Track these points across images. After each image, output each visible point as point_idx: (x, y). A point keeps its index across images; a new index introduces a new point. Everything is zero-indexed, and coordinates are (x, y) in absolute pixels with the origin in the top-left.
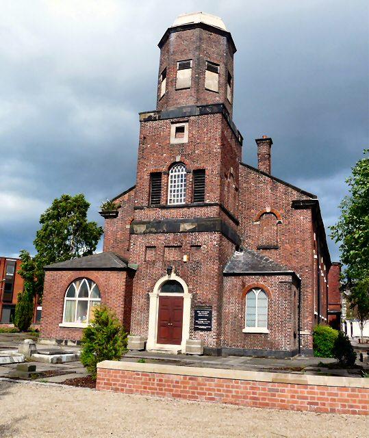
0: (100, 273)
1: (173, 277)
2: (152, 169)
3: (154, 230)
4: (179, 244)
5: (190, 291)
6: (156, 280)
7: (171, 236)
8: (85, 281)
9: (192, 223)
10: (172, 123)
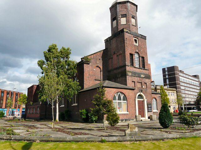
0: (126, 90)
1: (142, 94)
2: (130, 52)
3: (134, 75)
4: (141, 82)
5: (146, 99)
6: (136, 94)
7: (138, 78)
8: (119, 94)
9: (144, 75)
10: (134, 37)
